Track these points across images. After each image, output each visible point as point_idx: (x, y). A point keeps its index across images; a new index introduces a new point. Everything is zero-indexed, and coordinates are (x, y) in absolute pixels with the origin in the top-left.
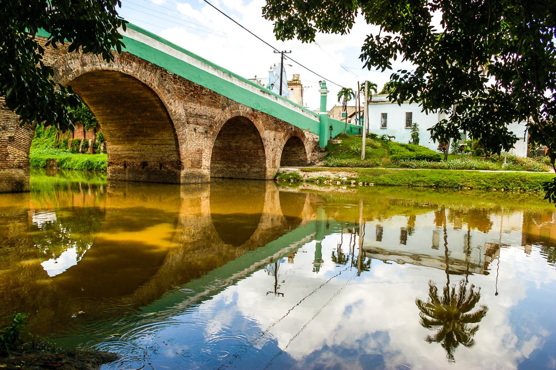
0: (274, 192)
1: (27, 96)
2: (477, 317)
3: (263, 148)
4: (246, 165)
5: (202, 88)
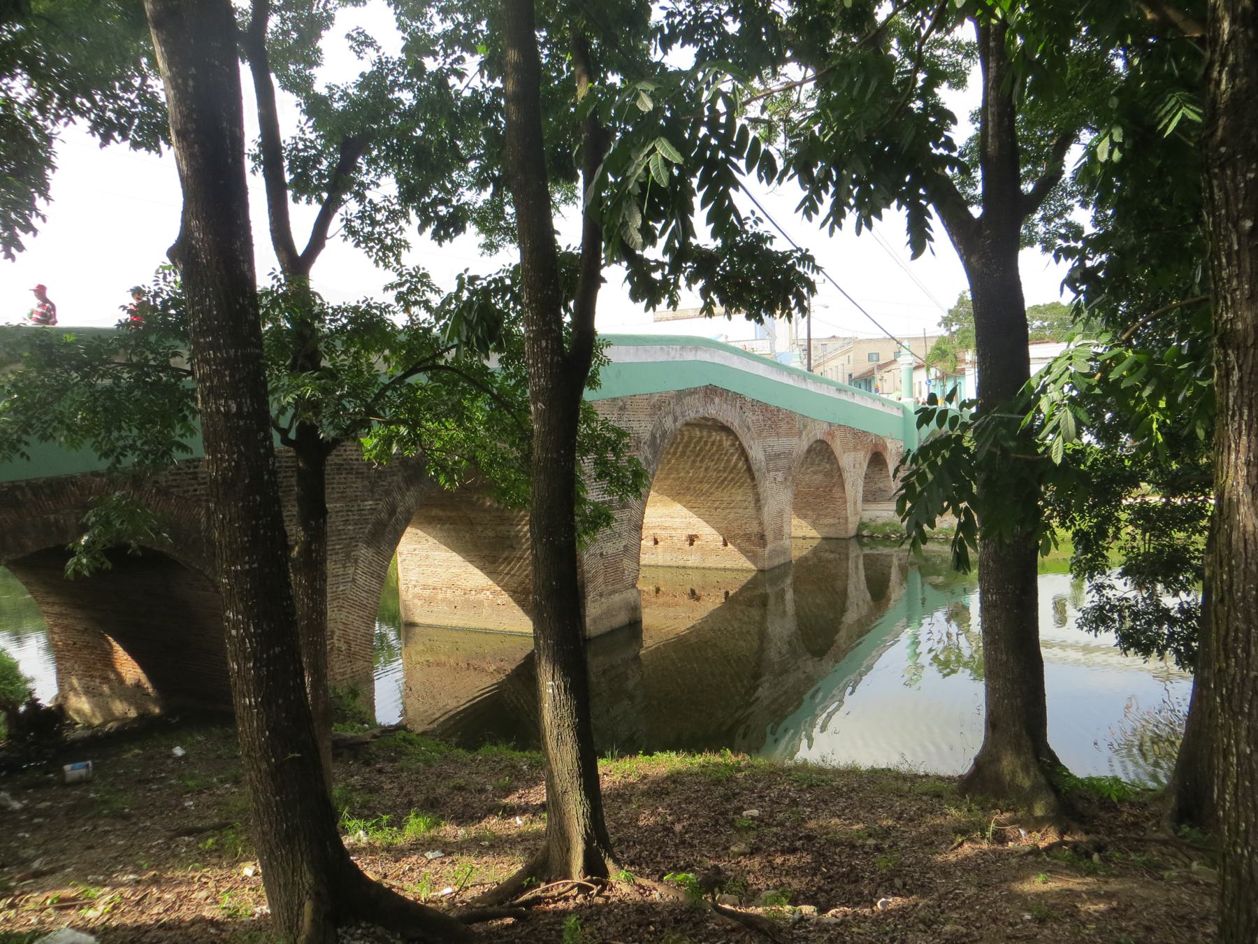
0: (858, 556)
1: (86, 538)
2: (376, 262)
3: (842, 486)
4: (809, 513)
5: (779, 410)
